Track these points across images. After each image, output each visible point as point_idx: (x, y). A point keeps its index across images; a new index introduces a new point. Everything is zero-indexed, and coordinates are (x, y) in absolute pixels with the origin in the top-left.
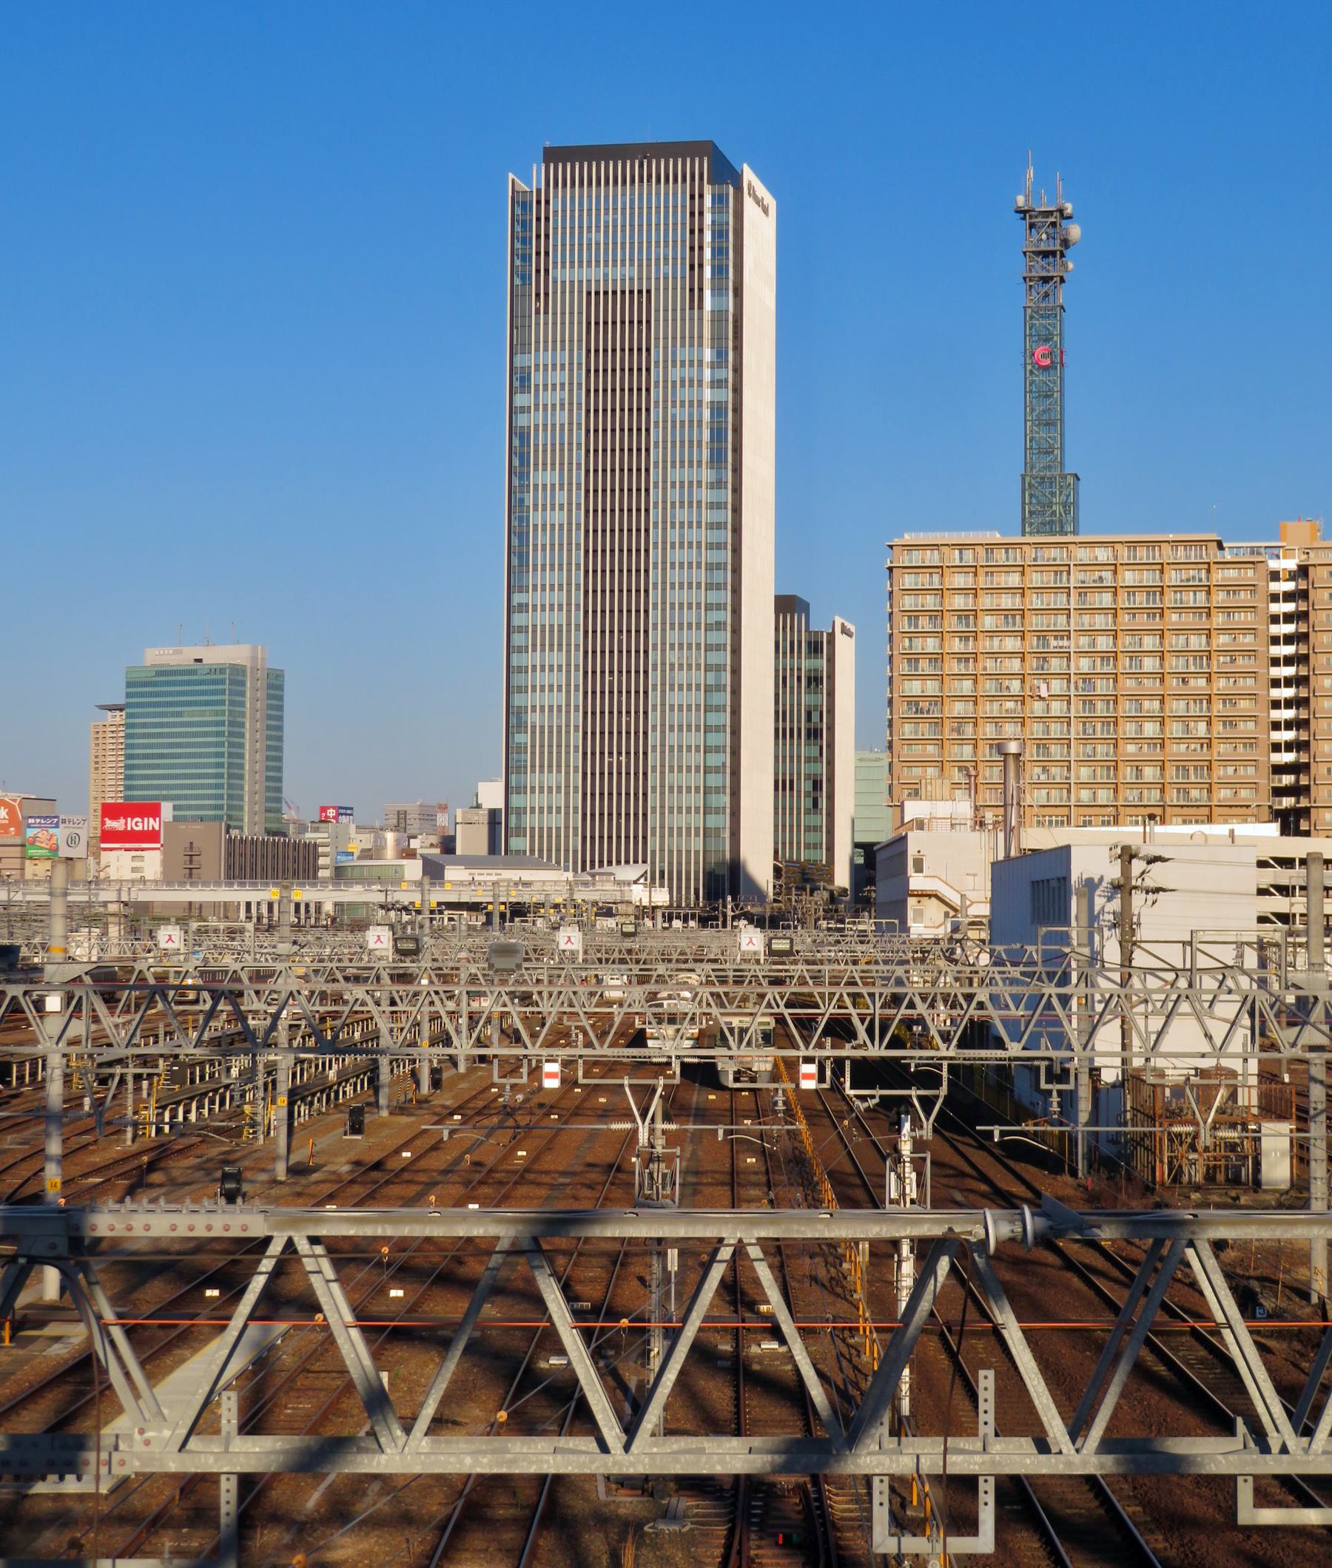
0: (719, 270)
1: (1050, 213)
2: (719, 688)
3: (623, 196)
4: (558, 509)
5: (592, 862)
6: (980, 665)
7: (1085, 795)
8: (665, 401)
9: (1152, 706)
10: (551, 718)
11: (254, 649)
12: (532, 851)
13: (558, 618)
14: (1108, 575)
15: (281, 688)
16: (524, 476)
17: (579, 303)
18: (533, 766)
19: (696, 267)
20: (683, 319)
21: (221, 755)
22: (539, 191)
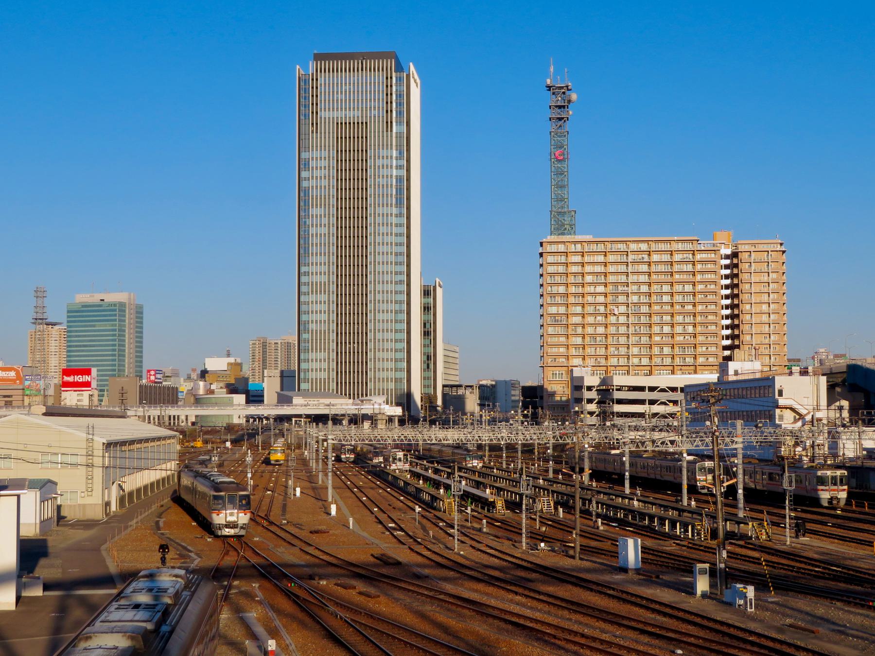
0: (400, 113)
1: (562, 88)
2: (401, 312)
3: (354, 77)
4: (323, 225)
5: (358, 394)
6: (586, 299)
7: (636, 361)
8: (375, 175)
9: (667, 318)
10: (321, 326)
11: (130, 295)
12: (312, 389)
13: (324, 279)
14: (646, 257)
15: (142, 313)
16: (307, 210)
17: (332, 128)
18: (312, 349)
19: (389, 111)
20: (383, 136)
21: (114, 345)
22: (313, 74)
